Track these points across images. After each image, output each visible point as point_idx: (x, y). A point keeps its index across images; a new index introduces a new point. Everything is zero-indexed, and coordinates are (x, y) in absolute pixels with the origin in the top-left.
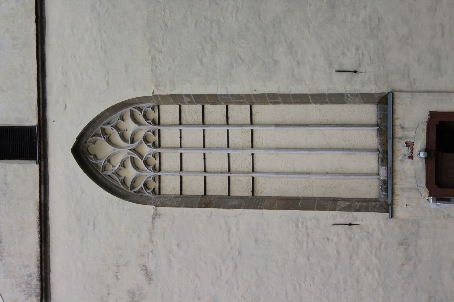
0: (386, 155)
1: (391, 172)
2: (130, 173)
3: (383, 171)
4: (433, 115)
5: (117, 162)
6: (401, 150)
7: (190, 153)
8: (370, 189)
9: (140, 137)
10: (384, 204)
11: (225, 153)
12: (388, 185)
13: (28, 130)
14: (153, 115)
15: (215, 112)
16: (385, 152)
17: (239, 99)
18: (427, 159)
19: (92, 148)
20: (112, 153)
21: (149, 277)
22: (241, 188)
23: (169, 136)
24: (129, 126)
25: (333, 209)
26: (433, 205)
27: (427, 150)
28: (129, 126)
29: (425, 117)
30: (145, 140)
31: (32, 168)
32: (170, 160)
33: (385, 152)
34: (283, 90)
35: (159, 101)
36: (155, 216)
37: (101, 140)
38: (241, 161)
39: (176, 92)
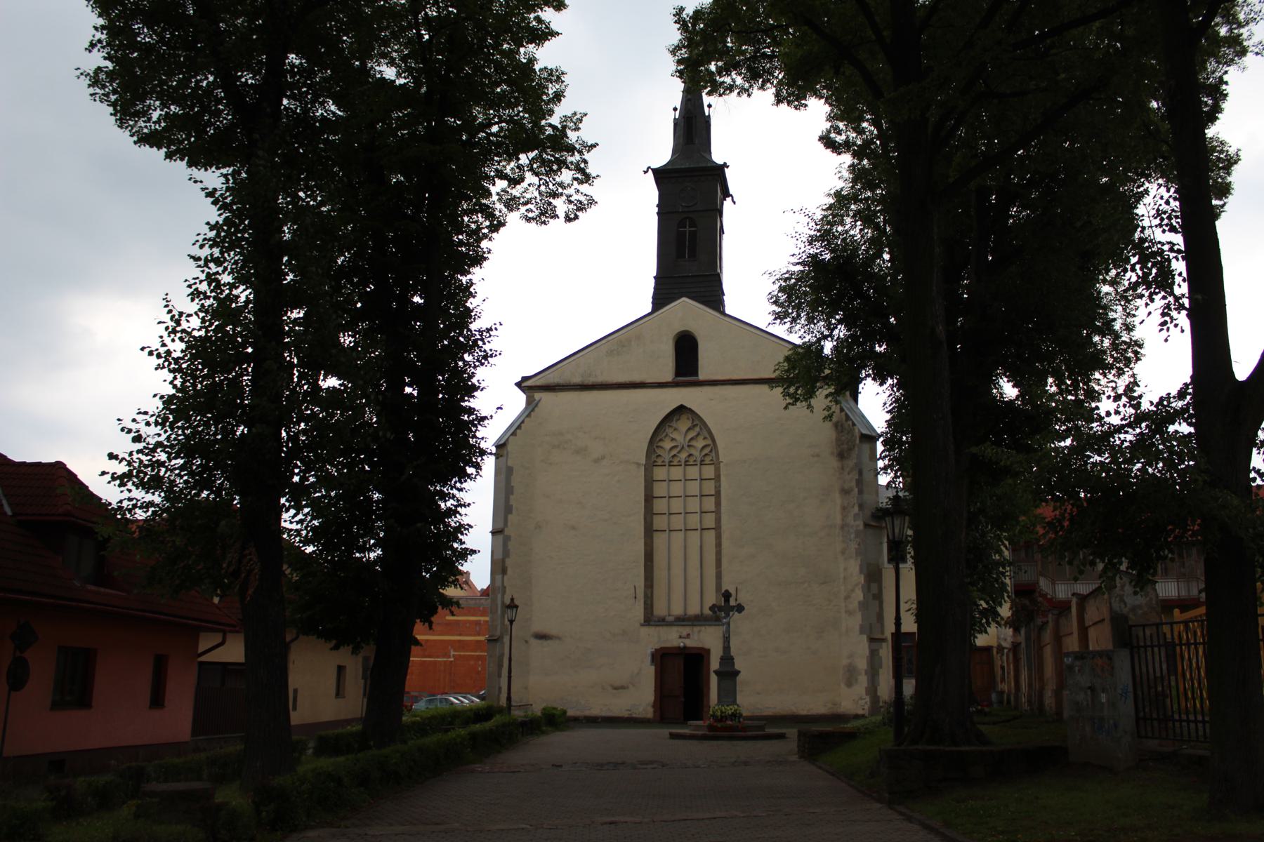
0: (682, 620)
1: (670, 624)
2: (667, 445)
3: (671, 619)
4: (708, 651)
5: (675, 435)
6: (685, 631)
7: (680, 485)
8: (660, 610)
9: (692, 451)
10: (650, 619)
11: (665, 527)
12: (662, 622)
13: (695, 373)
14: (707, 460)
15: (710, 504)
16: (683, 620)
17: (718, 520)
18: (679, 648)
19: (684, 417)
20: (680, 432)
21: (597, 461)
22: (659, 522)
23: (693, 472)
24: (700, 443)
25: (646, 586)
26: (649, 651)
27: (685, 647)
28: (700, 443)
29: (707, 646)
30: (690, 455)
31: (669, 376)
32: (677, 472)
33: (683, 620)
34: (724, 552)
35: (716, 464)
36: (638, 464)
37: (689, 424)
38: (677, 522)
39: (722, 478)
